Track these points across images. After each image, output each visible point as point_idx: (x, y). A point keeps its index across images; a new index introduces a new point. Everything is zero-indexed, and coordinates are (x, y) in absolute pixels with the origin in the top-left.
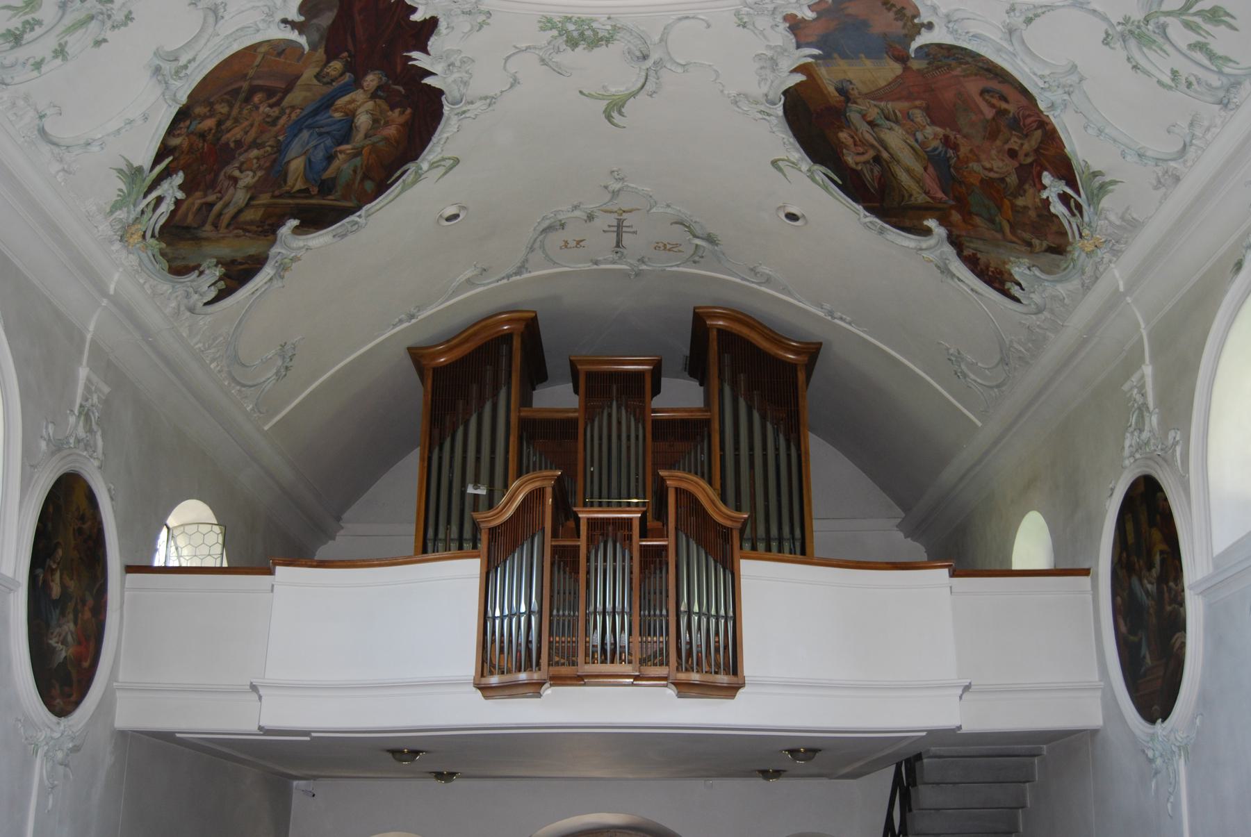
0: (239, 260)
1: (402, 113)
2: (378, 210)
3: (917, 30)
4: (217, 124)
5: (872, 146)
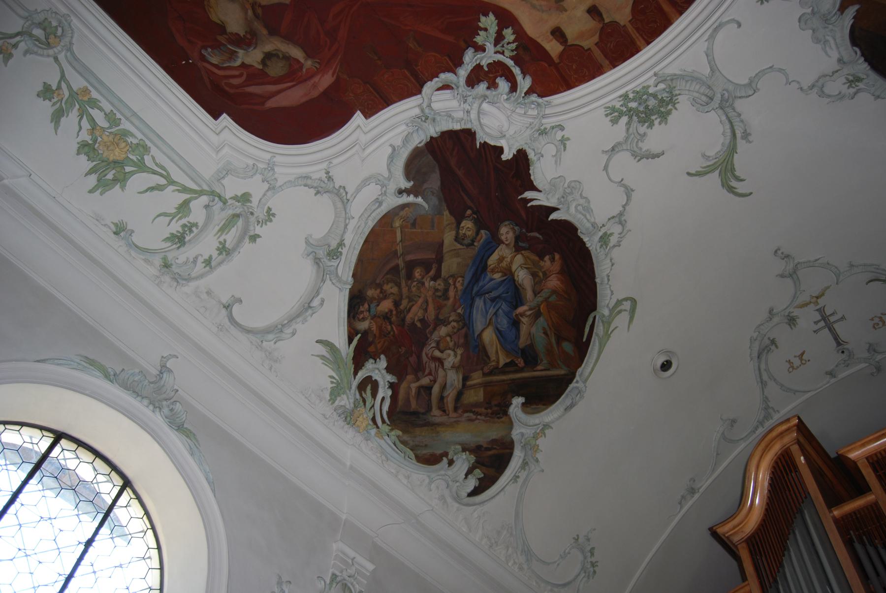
0: (485, 446)
1: (553, 260)
2: (591, 373)
4: (394, 305)
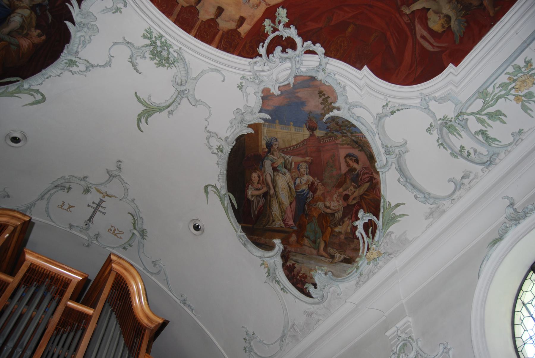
1: (39, 36)
3: (332, 109)
5: (268, 185)
